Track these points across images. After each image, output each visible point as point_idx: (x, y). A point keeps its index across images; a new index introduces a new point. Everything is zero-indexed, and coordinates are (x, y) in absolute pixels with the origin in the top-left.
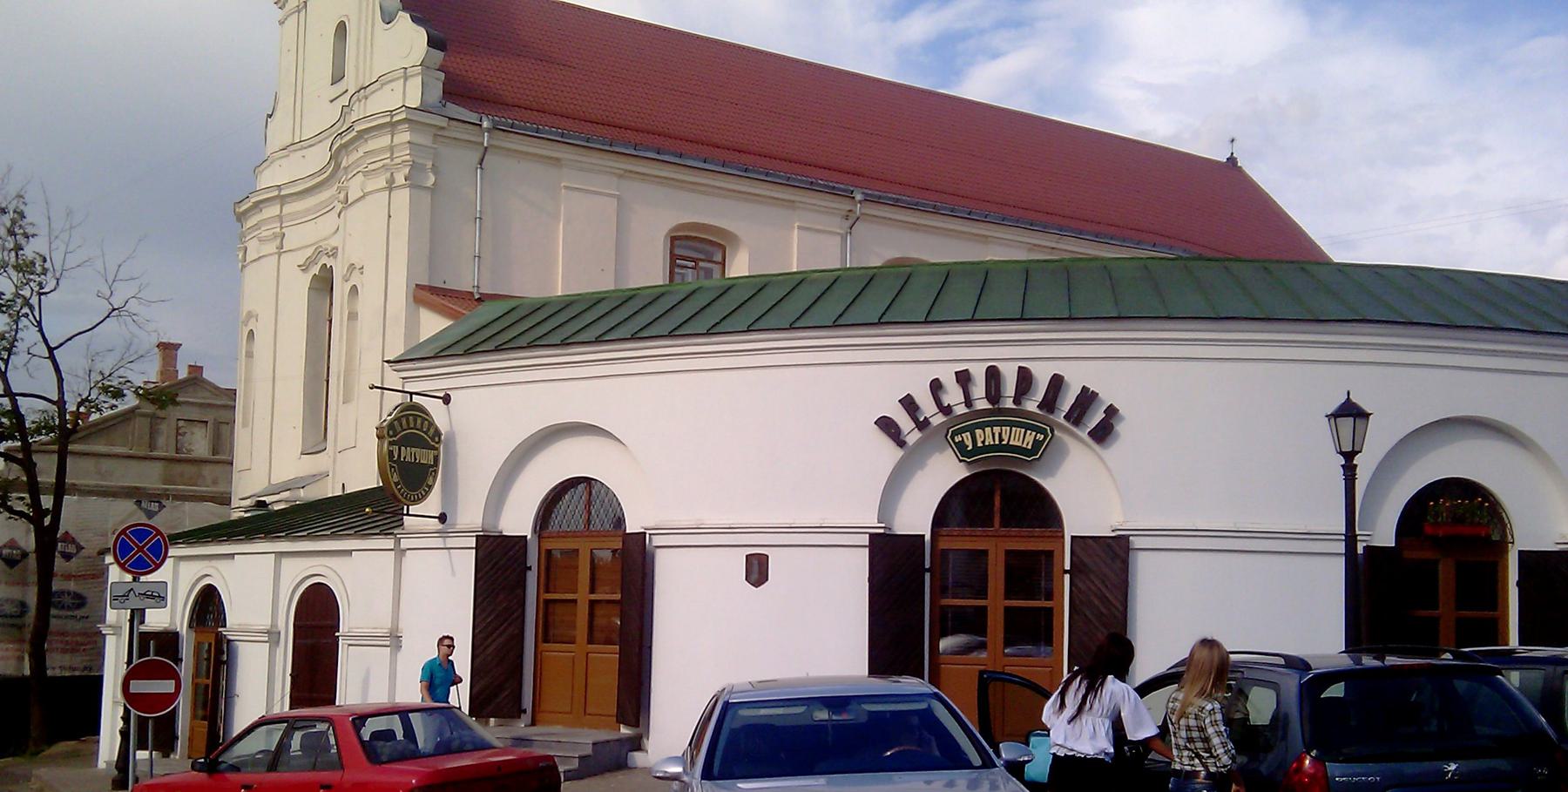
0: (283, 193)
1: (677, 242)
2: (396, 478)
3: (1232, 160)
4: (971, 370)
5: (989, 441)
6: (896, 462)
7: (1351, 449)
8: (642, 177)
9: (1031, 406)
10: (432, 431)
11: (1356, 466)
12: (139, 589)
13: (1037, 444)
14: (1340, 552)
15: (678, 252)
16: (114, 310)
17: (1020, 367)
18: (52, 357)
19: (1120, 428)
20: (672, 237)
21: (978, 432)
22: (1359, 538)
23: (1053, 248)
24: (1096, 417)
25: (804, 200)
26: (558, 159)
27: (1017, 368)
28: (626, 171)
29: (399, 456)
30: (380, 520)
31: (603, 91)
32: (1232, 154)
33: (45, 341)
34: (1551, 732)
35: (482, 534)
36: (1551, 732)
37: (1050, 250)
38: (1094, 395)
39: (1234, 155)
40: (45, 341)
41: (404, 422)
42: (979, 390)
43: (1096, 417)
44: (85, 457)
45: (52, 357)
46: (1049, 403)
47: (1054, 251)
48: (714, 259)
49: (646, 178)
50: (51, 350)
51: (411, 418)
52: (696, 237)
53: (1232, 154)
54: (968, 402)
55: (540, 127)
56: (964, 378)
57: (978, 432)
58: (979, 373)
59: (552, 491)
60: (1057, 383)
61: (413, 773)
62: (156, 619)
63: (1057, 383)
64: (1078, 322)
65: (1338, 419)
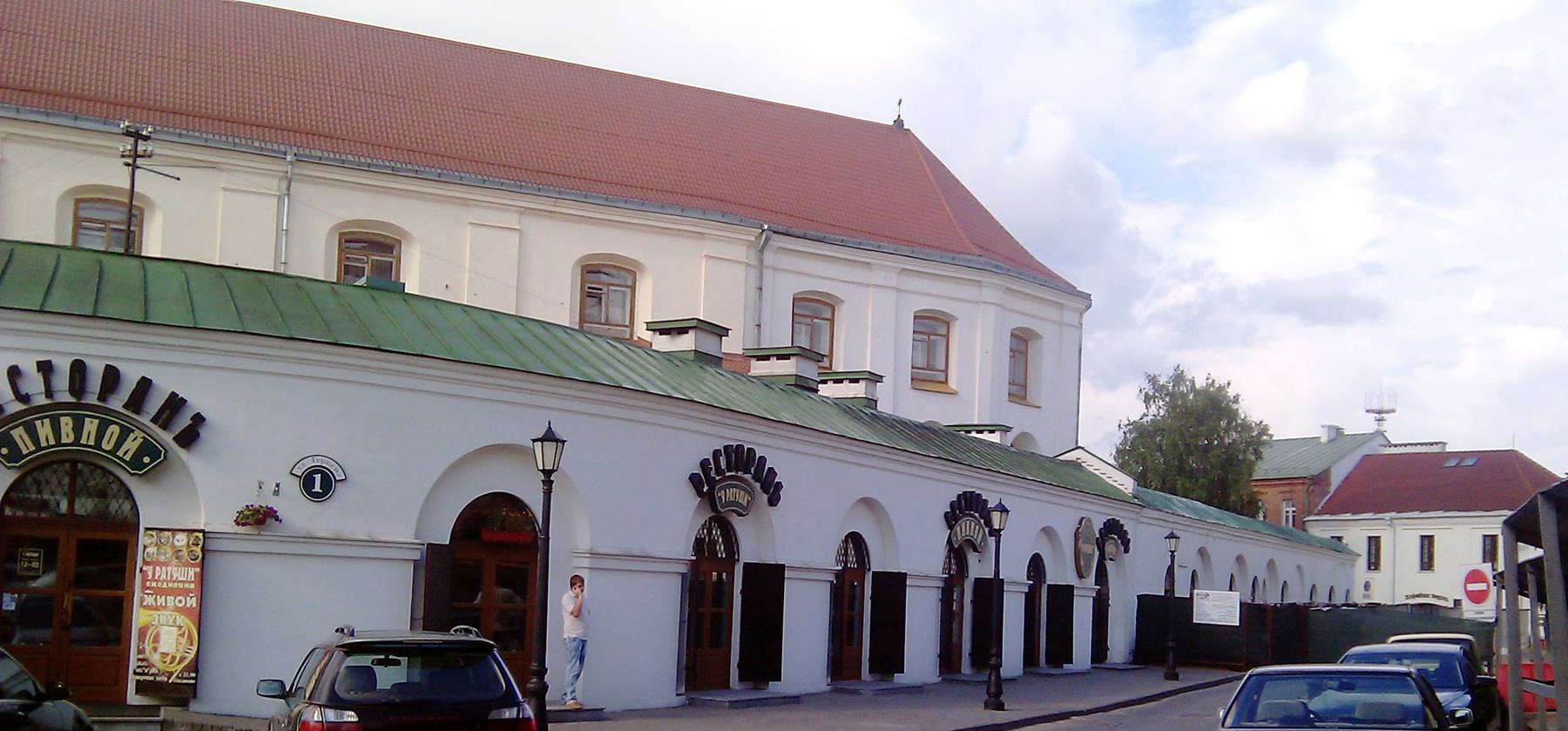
1: (82, 205)
3: (899, 122)
4: (53, 361)
11: (553, 481)
15: (83, 214)
17: (107, 365)
19: (204, 432)
24: (184, 421)
27: (104, 366)
30: (652, 373)
34: (29, 702)
36: (29, 702)
38: (183, 401)
39: (901, 117)
42: (62, 382)
43: (184, 421)
44: (762, 314)
47: (553, 214)
48: (823, 316)
51: (603, 321)
54: (49, 393)
56: (46, 368)
58: (63, 365)
60: (145, 385)
63: (145, 385)
65: (545, 443)
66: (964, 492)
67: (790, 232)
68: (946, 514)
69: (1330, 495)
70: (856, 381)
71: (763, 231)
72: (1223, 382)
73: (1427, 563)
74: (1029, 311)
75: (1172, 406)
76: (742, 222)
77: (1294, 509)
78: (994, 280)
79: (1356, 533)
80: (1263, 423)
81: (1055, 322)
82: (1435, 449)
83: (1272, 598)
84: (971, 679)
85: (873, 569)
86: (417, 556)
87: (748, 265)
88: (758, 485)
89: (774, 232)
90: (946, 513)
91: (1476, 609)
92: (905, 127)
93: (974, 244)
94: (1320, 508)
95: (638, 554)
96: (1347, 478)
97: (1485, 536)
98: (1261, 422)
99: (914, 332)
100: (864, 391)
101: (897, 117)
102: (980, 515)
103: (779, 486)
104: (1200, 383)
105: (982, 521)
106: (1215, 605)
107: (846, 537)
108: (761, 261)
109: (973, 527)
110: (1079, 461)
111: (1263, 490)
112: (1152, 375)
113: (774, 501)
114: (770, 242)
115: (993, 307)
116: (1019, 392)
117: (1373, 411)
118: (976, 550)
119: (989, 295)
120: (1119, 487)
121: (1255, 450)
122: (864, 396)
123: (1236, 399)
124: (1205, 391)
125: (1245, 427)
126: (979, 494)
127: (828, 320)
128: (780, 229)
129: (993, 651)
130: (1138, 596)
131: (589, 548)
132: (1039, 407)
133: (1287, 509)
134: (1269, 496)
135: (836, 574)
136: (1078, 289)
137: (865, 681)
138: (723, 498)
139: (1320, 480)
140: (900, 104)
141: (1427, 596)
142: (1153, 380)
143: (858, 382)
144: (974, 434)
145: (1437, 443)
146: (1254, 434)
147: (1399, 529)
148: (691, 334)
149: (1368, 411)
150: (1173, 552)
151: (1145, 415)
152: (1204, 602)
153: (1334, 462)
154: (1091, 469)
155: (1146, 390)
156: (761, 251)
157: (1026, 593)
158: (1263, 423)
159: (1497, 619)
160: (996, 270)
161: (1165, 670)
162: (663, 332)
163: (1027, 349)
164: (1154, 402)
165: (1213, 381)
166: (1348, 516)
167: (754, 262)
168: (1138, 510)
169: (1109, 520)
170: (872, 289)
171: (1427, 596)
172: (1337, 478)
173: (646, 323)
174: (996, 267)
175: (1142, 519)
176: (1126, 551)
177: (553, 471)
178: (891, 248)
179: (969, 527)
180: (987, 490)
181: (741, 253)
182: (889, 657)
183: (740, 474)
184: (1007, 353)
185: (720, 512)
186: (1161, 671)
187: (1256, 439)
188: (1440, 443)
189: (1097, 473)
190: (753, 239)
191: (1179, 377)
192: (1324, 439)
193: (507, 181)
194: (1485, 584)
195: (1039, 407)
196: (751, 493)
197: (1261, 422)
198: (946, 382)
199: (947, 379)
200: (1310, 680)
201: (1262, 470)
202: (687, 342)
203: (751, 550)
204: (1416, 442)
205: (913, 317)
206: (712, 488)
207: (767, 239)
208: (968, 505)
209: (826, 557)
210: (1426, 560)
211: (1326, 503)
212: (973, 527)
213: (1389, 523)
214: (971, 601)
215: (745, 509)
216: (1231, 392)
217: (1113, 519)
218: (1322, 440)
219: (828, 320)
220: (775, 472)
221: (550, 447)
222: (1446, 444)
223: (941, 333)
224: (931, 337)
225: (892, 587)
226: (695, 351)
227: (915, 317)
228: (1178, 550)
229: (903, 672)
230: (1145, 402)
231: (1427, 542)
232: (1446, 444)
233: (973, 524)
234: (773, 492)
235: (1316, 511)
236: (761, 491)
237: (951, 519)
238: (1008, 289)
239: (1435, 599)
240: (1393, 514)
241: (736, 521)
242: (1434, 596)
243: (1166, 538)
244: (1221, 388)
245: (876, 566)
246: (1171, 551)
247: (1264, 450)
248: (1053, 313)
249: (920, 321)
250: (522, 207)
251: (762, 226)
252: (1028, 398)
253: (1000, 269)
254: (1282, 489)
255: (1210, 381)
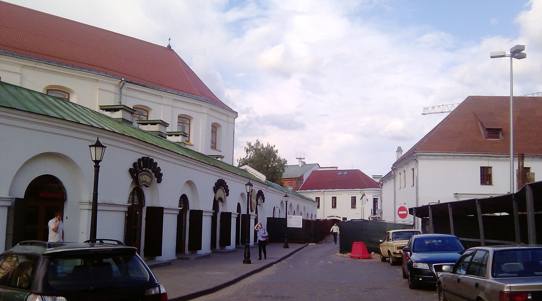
7: (99, 160)
8: (83, 78)
11: (100, 166)
14: (102, 213)
20: (47, 90)
22: (98, 204)
23: (35, 67)
25: (205, 105)
26: (201, 105)
31: (105, 61)
32: (169, 44)
35: (394, 223)
37: (33, 68)
47: (35, 68)
48: (144, 115)
49: (84, 78)
52: (67, 92)
53: (169, 44)
55: (146, 84)
61: (48, 251)
65: (97, 148)
66: (219, 179)
67: (133, 82)
68: (214, 187)
69: (303, 184)
70: (178, 135)
71: (122, 81)
72: (273, 146)
73: (334, 206)
74: (218, 118)
75: (256, 153)
76: (114, 76)
77: (292, 188)
78: (206, 105)
79: (312, 195)
80: (285, 160)
81: (226, 121)
82: (335, 169)
83: (481, 212)
84: (219, 251)
85: (190, 209)
86: (9, 204)
87: (115, 93)
88: (153, 174)
89: (126, 82)
90: (214, 187)
91: (402, 220)
92: (171, 49)
93: (199, 92)
94: (300, 188)
95: (109, 203)
96: (308, 178)
97: (352, 197)
98: (285, 159)
99: (178, 122)
100: (181, 140)
101: (168, 45)
102: (224, 188)
103: (161, 175)
104: (265, 146)
105: (224, 190)
106: (294, 221)
107: (180, 198)
108: (121, 92)
109: (222, 192)
110: (246, 169)
111: (284, 182)
112: (249, 143)
113: (159, 181)
114: (124, 85)
115: (206, 115)
116: (214, 146)
117: (298, 158)
118: (222, 201)
119: (205, 110)
120: (260, 179)
121: (283, 168)
122: (181, 141)
123: (277, 151)
124: (267, 148)
125: (279, 161)
126: (224, 180)
127: (146, 116)
128: (128, 80)
129: (247, 240)
130: (267, 218)
131: (89, 200)
132: (221, 151)
133: (290, 188)
134: (286, 183)
135: (179, 211)
136: (233, 110)
137: (187, 254)
138: (141, 179)
139: (301, 178)
140: (169, 40)
141: (334, 216)
142: (249, 144)
143: (179, 136)
144: (219, 159)
145: (335, 167)
146: (282, 163)
147: (325, 195)
148: (121, 111)
149: (297, 159)
150: (286, 202)
151: (247, 156)
152: (290, 220)
153: (304, 173)
154: (250, 172)
155: (247, 148)
156: (121, 88)
157: (236, 217)
158: (285, 160)
159: (414, 224)
160: (206, 101)
161: (284, 244)
162: (107, 110)
163: (216, 130)
164: (250, 152)
165: (269, 145)
166: (309, 191)
167: (118, 92)
168: (267, 187)
169: (259, 191)
170: (163, 106)
171: (334, 216)
172: (305, 179)
173: (100, 106)
174: (207, 100)
175: (268, 191)
176: (264, 202)
177: (100, 161)
178: (170, 91)
179: (221, 193)
180: (227, 179)
181: (113, 88)
182: (196, 244)
183: (147, 169)
184: (211, 132)
185: (140, 185)
186: (282, 245)
187: (282, 165)
188: (336, 167)
189: (253, 174)
190: (118, 83)
191: (258, 143)
192: (300, 166)
193: (16, 54)
194: (406, 212)
195: (221, 151)
196: (151, 177)
197: (285, 159)
198: (189, 141)
199: (189, 140)
200: (531, 251)
201: (285, 176)
202: (118, 115)
203: (150, 201)
204: (329, 167)
205: (177, 117)
206: (137, 175)
207: (124, 84)
208: (220, 185)
209: (175, 204)
210: (334, 205)
211: (302, 187)
212: (222, 192)
213: (360, 192)
214: (220, 221)
215: (149, 184)
216: (275, 149)
217: (261, 190)
218: (299, 166)
219: (146, 116)
220: (160, 169)
221: (99, 150)
222: (337, 167)
223: (187, 123)
224: (184, 124)
225: (197, 215)
226: (122, 118)
227: (178, 117)
228: (288, 201)
229: (201, 250)
230: (247, 152)
231: (334, 199)
232: (337, 167)
233: (222, 191)
234: (159, 177)
235: (299, 189)
236: (155, 177)
237: (215, 190)
238: (211, 108)
239: (337, 217)
240: (324, 190)
241: (144, 189)
242: (336, 216)
243: (284, 197)
244: (272, 148)
245: (191, 208)
246: (286, 201)
247: (286, 169)
248: (225, 118)
249: (180, 118)
250: (22, 64)
251: (121, 79)
252: (216, 148)
253: (208, 101)
254: (288, 182)
255: (268, 145)
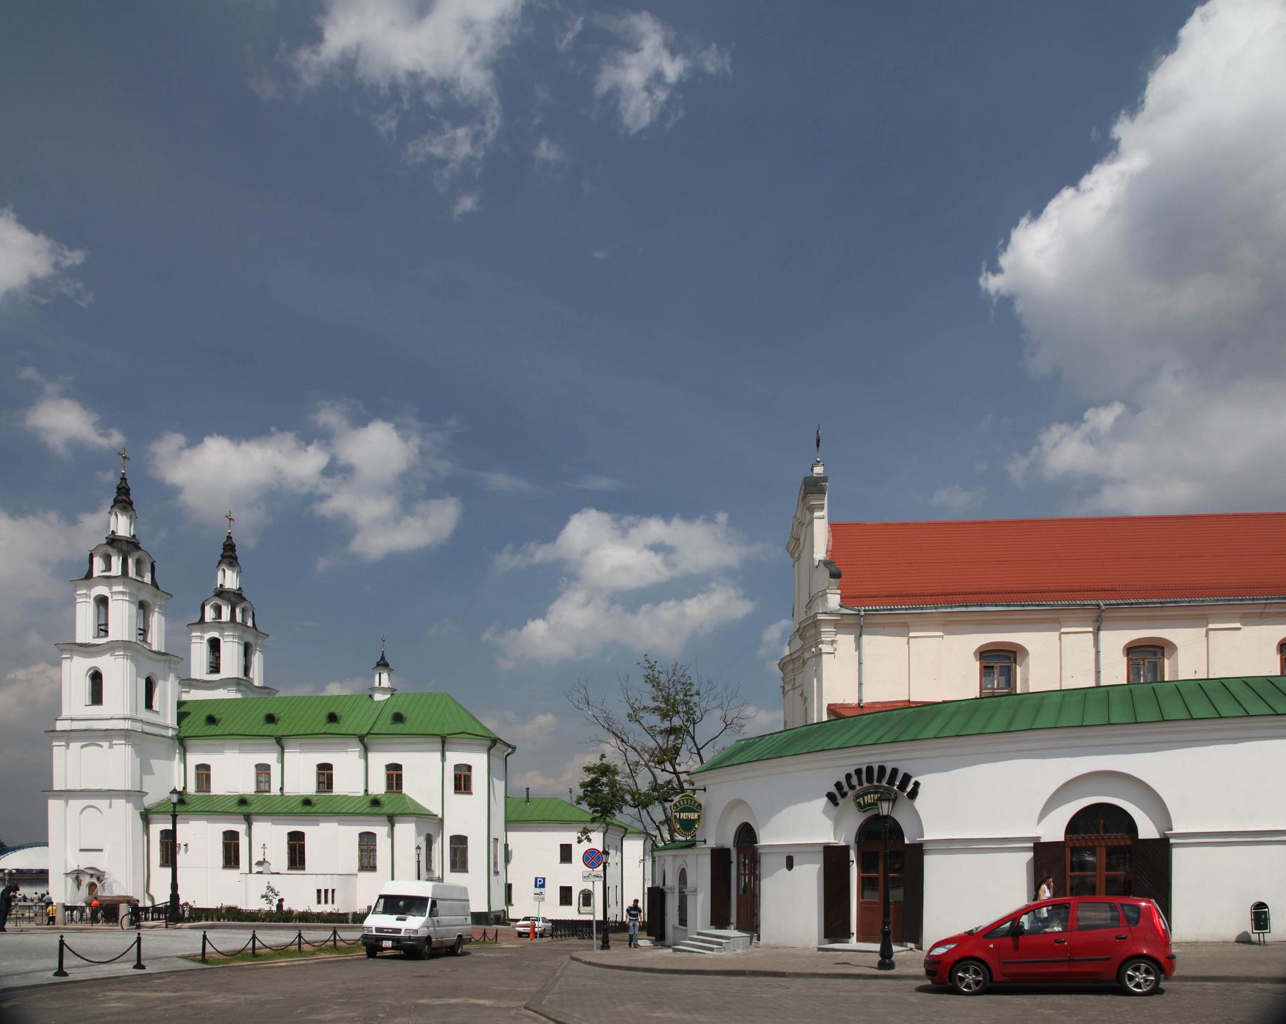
0: (793, 657)
2: (678, 826)
5: (870, 801)
6: (778, 815)
9: (884, 783)
10: (696, 804)
12: (593, 873)
13: (699, 816)
16: (727, 725)
18: (699, 754)
19: (921, 790)
21: (866, 797)
24: (910, 787)
28: (946, 621)
29: (680, 817)
33: (696, 745)
40: (696, 745)
41: (682, 802)
45: (699, 754)
46: (891, 782)
50: (698, 750)
57: (866, 797)
59: (738, 828)
60: (895, 771)
62: (1163, 975)
64: (902, 744)
